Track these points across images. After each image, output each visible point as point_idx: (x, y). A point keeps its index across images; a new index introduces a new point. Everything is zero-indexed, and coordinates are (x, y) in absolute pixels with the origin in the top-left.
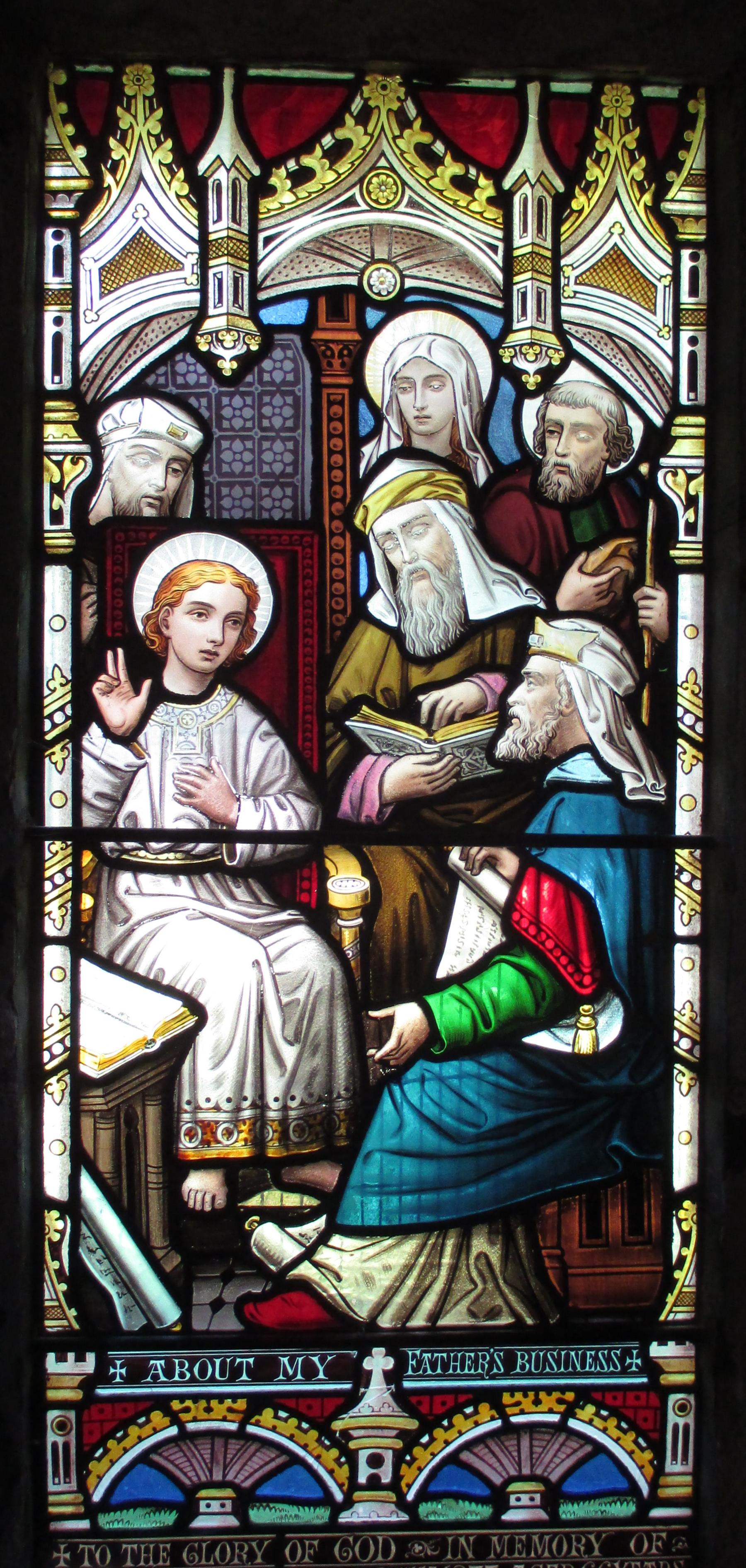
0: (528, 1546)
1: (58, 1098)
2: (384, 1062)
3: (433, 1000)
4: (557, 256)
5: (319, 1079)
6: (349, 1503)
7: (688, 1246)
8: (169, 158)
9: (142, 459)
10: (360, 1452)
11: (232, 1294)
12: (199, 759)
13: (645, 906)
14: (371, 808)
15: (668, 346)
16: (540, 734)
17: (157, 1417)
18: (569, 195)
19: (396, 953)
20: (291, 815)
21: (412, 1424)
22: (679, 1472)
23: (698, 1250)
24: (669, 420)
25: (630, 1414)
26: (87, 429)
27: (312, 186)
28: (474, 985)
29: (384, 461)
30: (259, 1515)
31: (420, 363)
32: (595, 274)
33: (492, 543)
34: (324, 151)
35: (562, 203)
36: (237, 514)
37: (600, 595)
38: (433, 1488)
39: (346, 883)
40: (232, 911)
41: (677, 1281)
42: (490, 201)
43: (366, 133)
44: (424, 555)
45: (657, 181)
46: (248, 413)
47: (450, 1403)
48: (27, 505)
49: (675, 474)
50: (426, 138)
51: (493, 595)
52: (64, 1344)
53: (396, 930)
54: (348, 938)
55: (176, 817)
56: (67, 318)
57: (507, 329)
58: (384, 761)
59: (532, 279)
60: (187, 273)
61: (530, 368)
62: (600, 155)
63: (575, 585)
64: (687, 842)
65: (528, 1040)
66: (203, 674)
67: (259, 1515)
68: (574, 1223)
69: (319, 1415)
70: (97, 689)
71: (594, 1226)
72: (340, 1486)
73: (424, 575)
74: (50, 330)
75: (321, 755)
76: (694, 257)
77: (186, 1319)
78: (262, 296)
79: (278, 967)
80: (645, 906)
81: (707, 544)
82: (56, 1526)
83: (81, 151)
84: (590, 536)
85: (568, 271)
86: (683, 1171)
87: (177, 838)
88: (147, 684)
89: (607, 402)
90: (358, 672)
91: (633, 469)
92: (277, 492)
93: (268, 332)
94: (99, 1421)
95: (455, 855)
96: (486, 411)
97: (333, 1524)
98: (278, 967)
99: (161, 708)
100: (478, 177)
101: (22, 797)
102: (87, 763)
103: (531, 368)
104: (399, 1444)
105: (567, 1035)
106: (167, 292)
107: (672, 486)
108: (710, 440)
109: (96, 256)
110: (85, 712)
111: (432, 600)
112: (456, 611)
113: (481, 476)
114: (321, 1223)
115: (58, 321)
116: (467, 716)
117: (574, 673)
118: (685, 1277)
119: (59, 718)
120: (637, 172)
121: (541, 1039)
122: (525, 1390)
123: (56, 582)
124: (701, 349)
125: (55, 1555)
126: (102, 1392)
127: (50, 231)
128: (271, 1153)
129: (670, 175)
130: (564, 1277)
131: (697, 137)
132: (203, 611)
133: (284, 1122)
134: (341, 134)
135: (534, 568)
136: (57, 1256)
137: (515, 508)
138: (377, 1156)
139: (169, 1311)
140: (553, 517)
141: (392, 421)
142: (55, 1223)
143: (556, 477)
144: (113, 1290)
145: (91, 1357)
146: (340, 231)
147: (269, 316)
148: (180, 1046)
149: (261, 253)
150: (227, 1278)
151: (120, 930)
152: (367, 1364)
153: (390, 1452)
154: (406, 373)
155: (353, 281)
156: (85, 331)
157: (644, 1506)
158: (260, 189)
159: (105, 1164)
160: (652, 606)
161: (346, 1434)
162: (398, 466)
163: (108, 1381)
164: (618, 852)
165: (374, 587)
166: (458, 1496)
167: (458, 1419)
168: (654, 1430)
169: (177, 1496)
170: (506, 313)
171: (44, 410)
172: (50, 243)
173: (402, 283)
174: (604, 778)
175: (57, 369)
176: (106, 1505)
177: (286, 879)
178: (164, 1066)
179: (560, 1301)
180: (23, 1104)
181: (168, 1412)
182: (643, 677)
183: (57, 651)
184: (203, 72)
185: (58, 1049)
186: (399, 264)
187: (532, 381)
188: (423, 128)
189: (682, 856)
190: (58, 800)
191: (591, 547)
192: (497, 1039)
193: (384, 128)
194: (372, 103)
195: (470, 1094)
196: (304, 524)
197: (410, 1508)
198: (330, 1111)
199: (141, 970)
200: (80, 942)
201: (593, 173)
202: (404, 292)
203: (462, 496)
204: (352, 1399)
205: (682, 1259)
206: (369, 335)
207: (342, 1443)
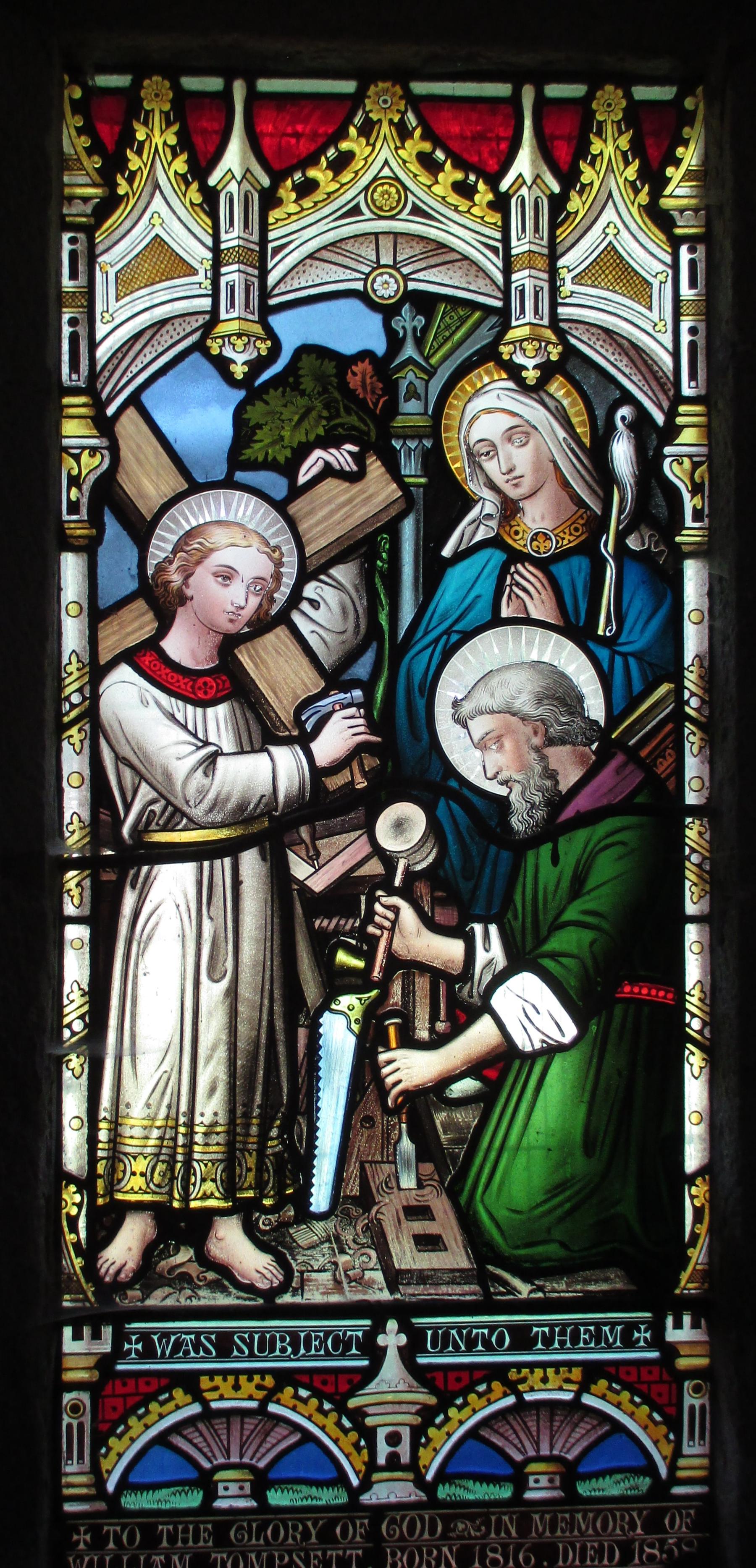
1: (78, 1071)
6: (366, 1484)
7: (701, 1223)
10: (379, 1430)
15: (667, 339)
21: (432, 1400)
22: (694, 1451)
23: (711, 1230)
25: (644, 1388)
34: (328, 162)
35: (558, 203)
38: (450, 1470)
41: (690, 1258)
42: (491, 205)
43: (368, 144)
45: (653, 178)
47: (466, 1381)
48: (53, 790)
49: (681, 464)
56: (83, 318)
59: (530, 276)
60: (200, 277)
62: (594, 157)
72: (357, 1473)
76: (692, 250)
85: (563, 272)
86: (694, 1156)
94: (118, 1395)
100: (476, 182)
104: (417, 1420)
106: (185, 297)
108: (709, 430)
109: (113, 259)
115: (73, 322)
125: (75, 1537)
134: (344, 146)
136: (74, 1229)
145: (107, 1332)
153: (408, 1429)
156: (101, 330)
158: (269, 200)
168: (670, 1404)
171: (63, 407)
173: (406, 286)
175: (74, 366)
186: (402, 270)
188: (423, 138)
194: (374, 116)
197: (429, 1489)
201: (588, 174)
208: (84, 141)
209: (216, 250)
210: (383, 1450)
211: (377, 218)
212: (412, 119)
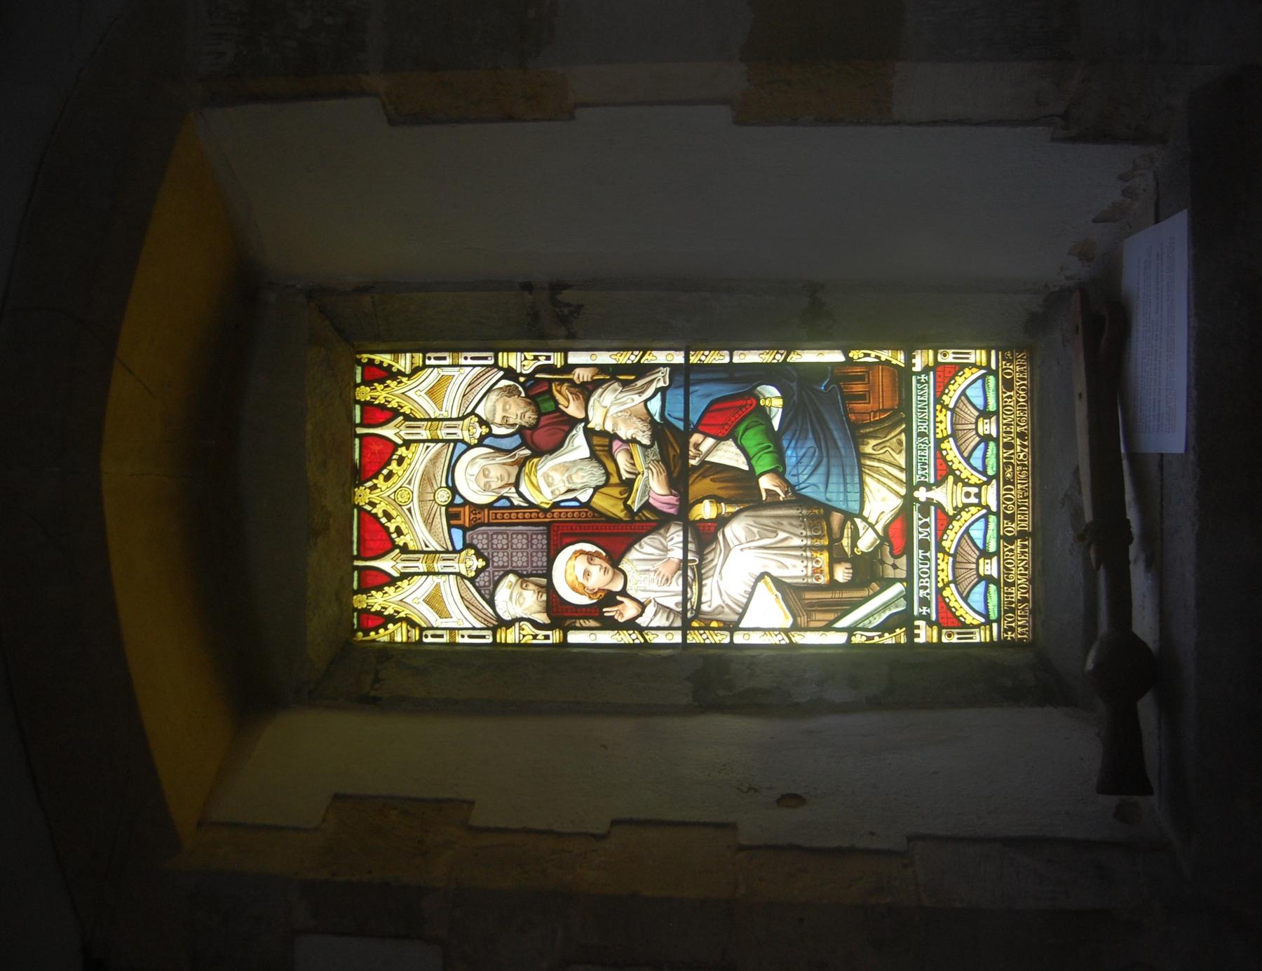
0: (1008, 425)
2: (786, 493)
3: (758, 471)
4: (430, 420)
5: (795, 522)
6: (987, 507)
8: (393, 588)
9: (521, 600)
11: (890, 560)
12: (650, 574)
13: (716, 376)
14: (673, 500)
16: (640, 424)
17: (945, 593)
18: (404, 414)
19: (737, 488)
20: (675, 535)
21: (951, 479)
22: (977, 356)
24: (501, 369)
26: (509, 624)
27: (403, 527)
28: (751, 452)
29: (521, 495)
30: (992, 547)
31: (479, 479)
32: (438, 402)
33: (556, 447)
35: (407, 418)
36: (545, 559)
37: (578, 398)
39: (706, 510)
40: (718, 561)
44: (561, 477)
46: (501, 554)
48: (542, 649)
50: (381, 477)
51: (578, 446)
52: (911, 635)
53: (726, 488)
54: (731, 509)
55: (677, 585)
57: (462, 441)
58: (652, 494)
61: (480, 431)
63: (574, 410)
64: (687, 358)
65: (776, 428)
66: (614, 573)
67: (992, 547)
68: (859, 406)
69: (945, 520)
70: (621, 620)
71: (862, 397)
73: (570, 478)
74: (467, 640)
75: (646, 523)
77: (901, 580)
78: (450, 548)
79: (743, 540)
80: (716, 376)
81: (554, 351)
82: (995, 639)
83: (390, 626)
84: (552, 403)
86: (836, 357)
87: (686, 585)
88: (619, 598)
89: (493, 396)
90: (613, 506)
91: (522, 384)
92: (535, 541)
93: (466, 546)
94: (947, 619)
95: (693, 462)
96: (498, 450)
97: (997, 514)
98: (743, 540)
99: (629, 592)
101: (669, 652)
102: (653, 624)
103: (479, 430)
104: (960, 484)
105: (774, 409)
106: (449, 588)
107: (529, 367)
109: (436, 621)
110: (631, 625)
111: (581, 474)
112: (586, 462)
113: (527, 452)
114: (858, 521)
116: (632, 458)
117: (613, 410)
118: (885, 355)
119: (634, 636)
120: (393, 384)
121: (776, 423)
122: (935, 427)
123: (574, 637)
124: (432, 355)
126: (934, 617)
127: (425, 640)
128: (826, 543)
129: (394, 370)
130: (885, 411)
131: (378, 358)
132: (587, 574)
133: (812, 537)
134: (380, 515)
135: (566, 428)
136: (872, 638)
137: (541, 437)
138: (828, 495)
139: (898, 588)
140: (544, 420)
141: (504, 492)
142: (858, 639)
143: (526, 419)
144: (888, 613)
145: (917, 623)
146: (422, 515)
147: (459, 546)
148: (779, 583)
149: (431, 549)
150: (883, 562)
151: (727, 610)
152: (923, 499)
154: (482, 484)
155: (443, 509)
157: (990, 372)
158: (405, 549)
159: (831, 616)
160: (582, 375)
161: (955, 508)
162: (523, 489)
163: (929, 615)
164: (692, 389)
165: (575, 499)
166: (984, 457)
167: (948, 458)
169: (983, 583)
170: (456, 442)
172: (430, 640)
174: (659, 396)
175: (484, 637)
176: (986, 615)
177: (704, 537)
178: (789, 591)
179: (895, 412)
180: (803, 651)
181: (943, 588)
182: (614, 378)
183: (606, 637)
184: (356, 574)
185: (780, 637)
187: (485, 430)
189: (694, 359)
190: (670, 637)
191: (557, 403)
192: (775, 441)
193: (376, 496)
195: (803, 451)
196: (549, 530)
197: (990, 479)
198: (807, 517)
199: (745, 601)
200: (732, 627)
201: (394, 404)
202: (448, 487)
203: (535, 460)
204: (939, 507)
205: (877, 357)
206: (466, 502)
207: (959, 510)
208: (381, 631)
209: (428, 574)
210: (973, 500)
211: (402, 498)
212: (369, 484)
